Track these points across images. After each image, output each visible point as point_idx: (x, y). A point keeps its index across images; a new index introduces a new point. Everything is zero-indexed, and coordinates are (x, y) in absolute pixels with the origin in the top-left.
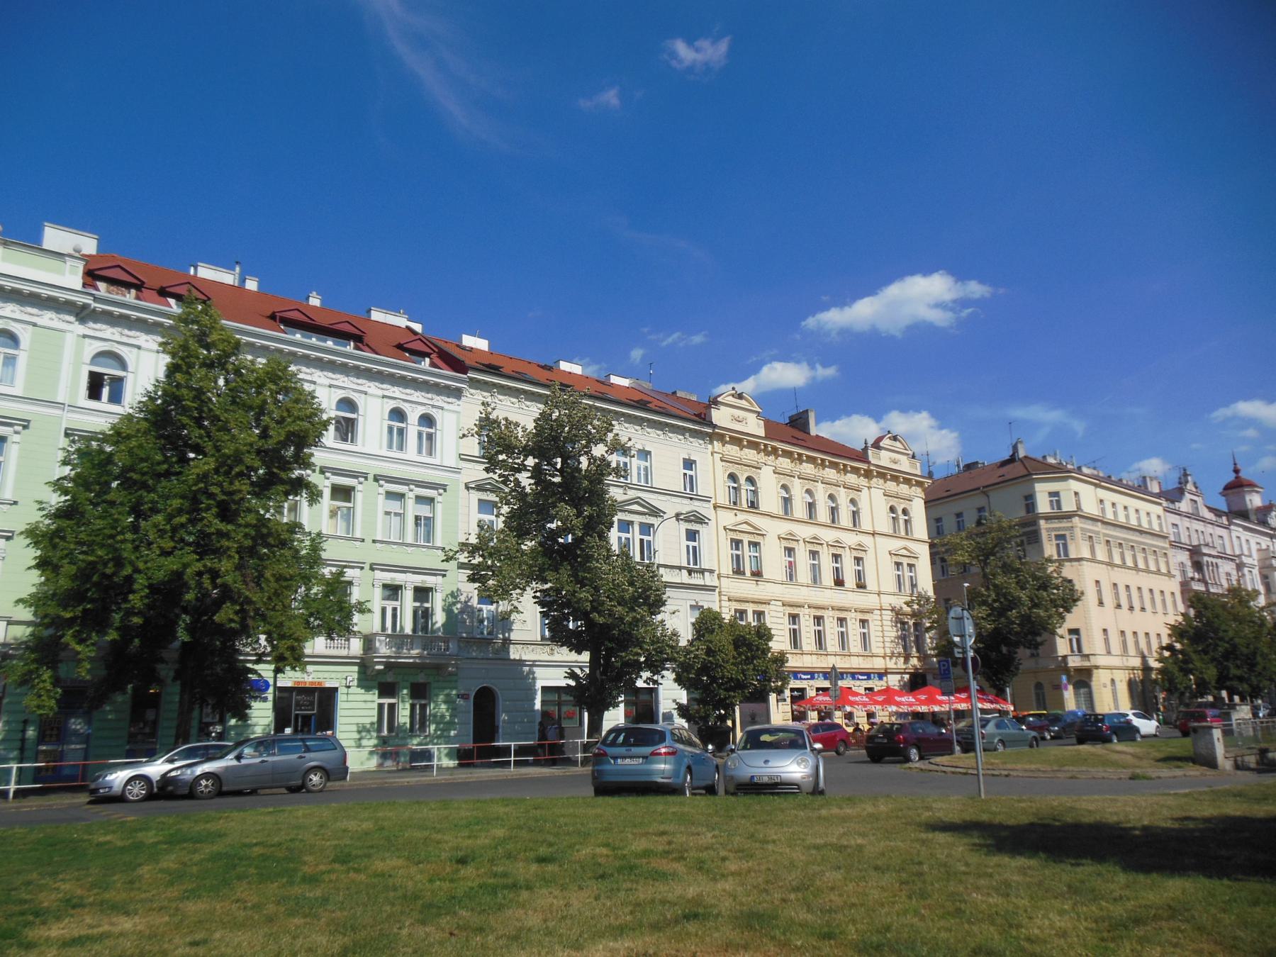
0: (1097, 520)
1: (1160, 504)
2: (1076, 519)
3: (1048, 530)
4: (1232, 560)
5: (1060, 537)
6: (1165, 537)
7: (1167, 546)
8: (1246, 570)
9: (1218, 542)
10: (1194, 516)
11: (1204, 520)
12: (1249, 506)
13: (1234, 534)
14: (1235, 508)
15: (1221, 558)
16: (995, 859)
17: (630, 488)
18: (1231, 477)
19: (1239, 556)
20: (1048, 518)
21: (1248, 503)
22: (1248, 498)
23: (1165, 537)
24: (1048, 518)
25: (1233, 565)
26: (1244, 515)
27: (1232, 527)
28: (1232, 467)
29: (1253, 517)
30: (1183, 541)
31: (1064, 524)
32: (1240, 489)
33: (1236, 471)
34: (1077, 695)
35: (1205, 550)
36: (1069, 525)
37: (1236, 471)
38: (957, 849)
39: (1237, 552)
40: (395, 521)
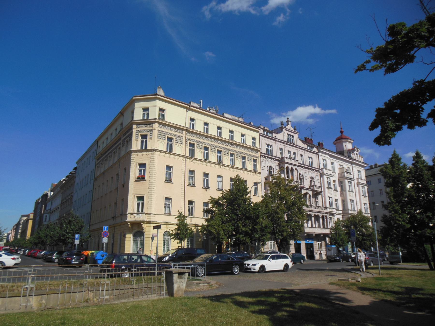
0: (183, 130)
1: (258, 132)
2: (156, 125)
3: (137, 131)
4: (316, 171)
5: (144, 137)
6: (257, 151)
7: (259, 155)
8: (325, 177)
9: (299, 159)
10: (290, 142)
11: (297, 147)
12: (345, 149)
13: (321, 159)
14: (339, 150)
15: (300, 166)
16: (231, 304)
17: (187, 158)
18: (339, 135)
19: (322, 169)
20: (139, 124)
21: (344, 147)
22: (344, 145)
23: (257, 151)
24: (139, 124)
25: (318, 174)
26: (341, 153)
27: (320, 154)
28: (340, 130)
29: (346, 154)
30: (274, 155)
31: (148, 128)
32: (340, 140)
33: (342, 132)
34: (135, 241)
35: (286, 160)
36: (151, 128)
37: (342, 132)
38: (208, 301)
39: (322, 167)
40: (220, 183)
